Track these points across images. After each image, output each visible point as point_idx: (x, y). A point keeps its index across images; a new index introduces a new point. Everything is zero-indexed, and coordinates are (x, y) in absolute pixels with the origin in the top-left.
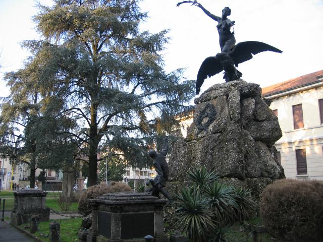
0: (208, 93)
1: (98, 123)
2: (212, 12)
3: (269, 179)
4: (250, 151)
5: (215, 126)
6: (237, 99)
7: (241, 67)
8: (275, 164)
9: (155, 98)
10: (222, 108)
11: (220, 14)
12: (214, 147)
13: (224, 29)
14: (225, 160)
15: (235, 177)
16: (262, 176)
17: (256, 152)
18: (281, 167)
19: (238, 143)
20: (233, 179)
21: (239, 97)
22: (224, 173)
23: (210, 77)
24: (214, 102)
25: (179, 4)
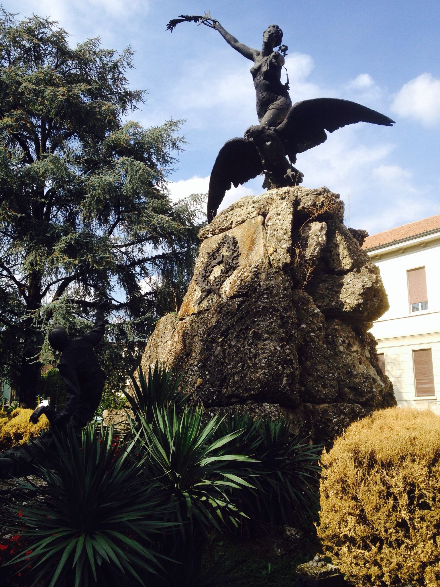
0: (227, 214)
1: (44, 294)
2: (242, 41)
3: (357, 408)
4: (312, 340)
5: (235, 282)
6: (286, 221)
7: (305, 161)
8: (372, 372)
9: (149, 250)
10: (253, 242)
11: (257, 45)
12: (228, 329)
13: (266, 75)
14: (250, 359)
15: (272, 402)
16: (340, 397)
17: (327, 342)
18: (385, 379)
19: (282, 318)
20: (267, 406)
21: (291, 216)
22: (246, 390)
23: (236, 186)
24: (237, 232)
25: (173, 24)
